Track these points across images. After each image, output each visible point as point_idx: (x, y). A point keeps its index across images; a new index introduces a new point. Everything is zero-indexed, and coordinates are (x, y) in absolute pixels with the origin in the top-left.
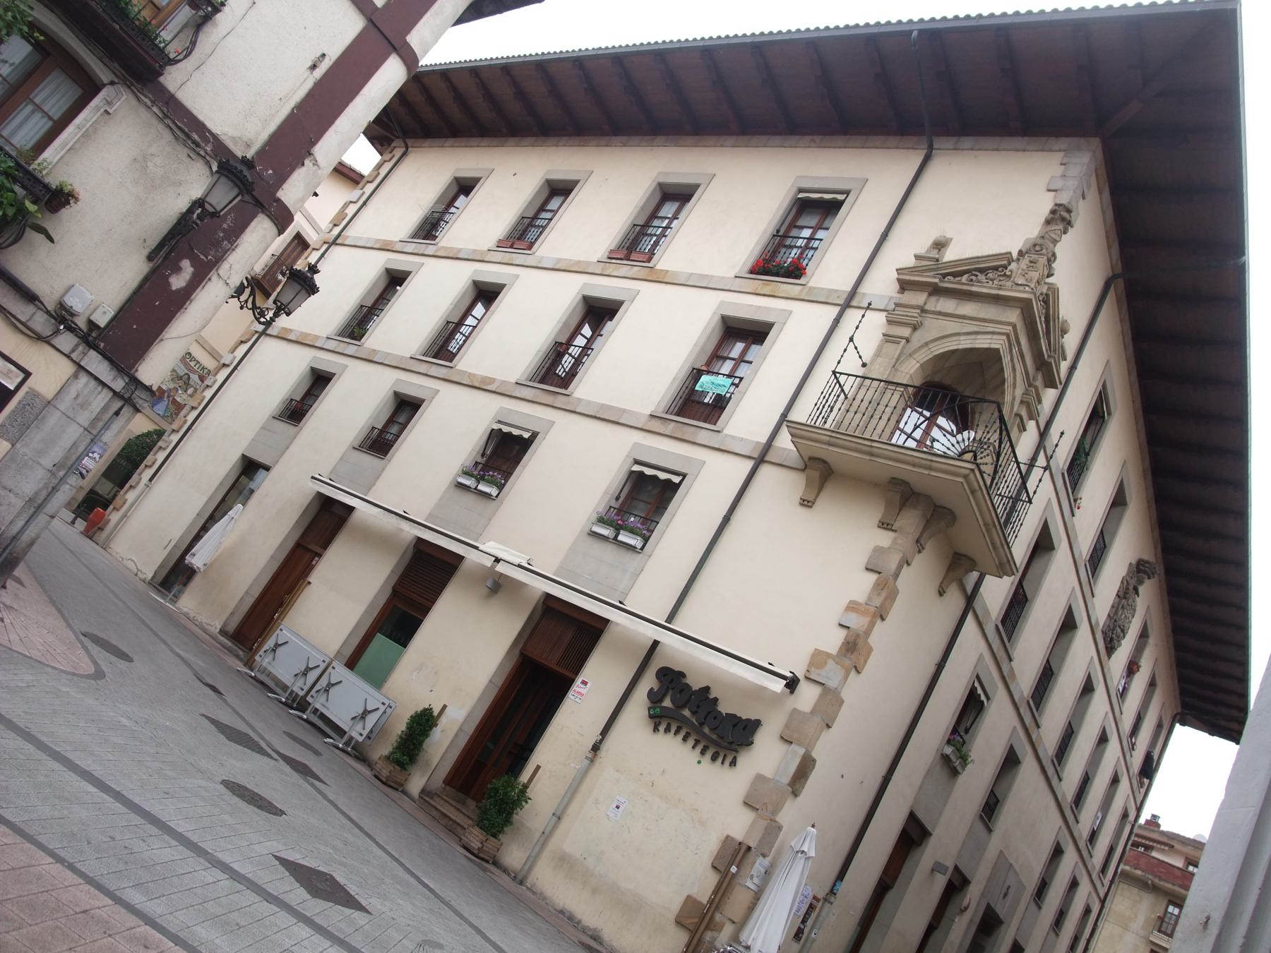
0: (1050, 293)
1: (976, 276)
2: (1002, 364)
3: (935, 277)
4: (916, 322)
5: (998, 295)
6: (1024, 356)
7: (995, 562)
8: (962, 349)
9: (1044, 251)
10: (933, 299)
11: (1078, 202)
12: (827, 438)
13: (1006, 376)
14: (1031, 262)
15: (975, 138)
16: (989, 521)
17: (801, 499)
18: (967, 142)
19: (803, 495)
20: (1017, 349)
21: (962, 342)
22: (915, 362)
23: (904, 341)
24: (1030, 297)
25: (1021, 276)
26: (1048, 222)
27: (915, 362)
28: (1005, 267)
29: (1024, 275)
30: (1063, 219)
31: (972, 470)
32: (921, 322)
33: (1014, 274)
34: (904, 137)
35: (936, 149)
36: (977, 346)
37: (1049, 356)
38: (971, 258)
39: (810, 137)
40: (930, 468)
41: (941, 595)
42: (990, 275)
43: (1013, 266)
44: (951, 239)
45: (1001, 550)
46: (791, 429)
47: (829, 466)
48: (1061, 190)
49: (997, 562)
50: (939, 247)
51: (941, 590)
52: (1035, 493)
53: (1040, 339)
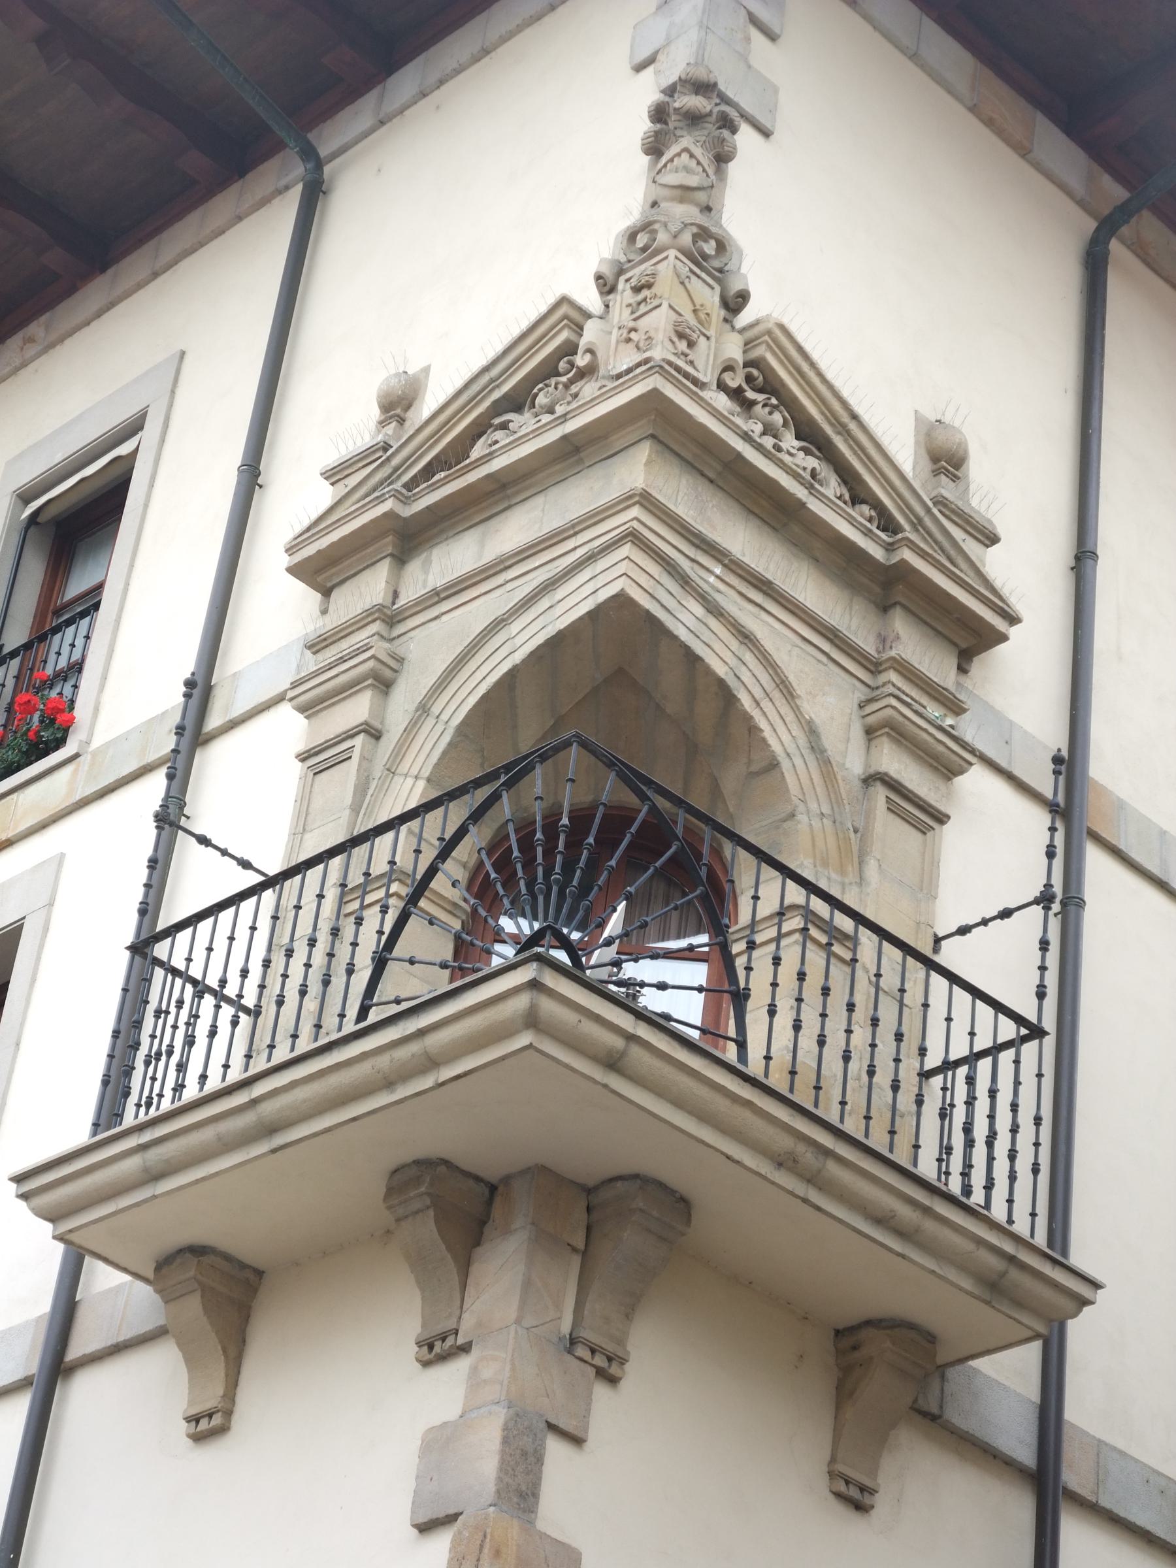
0: (760, 351)
1: (504, 426)
2: (675, 638)
3: (381, 500)
4: (371, 663)
5: (565, 438)
6: (769, 583)
7: (961, 1289)
8: (525, 661)
9: (662, 237)
10: (414, 568)
11: (744, 58)
12: (133, 1164)
13: (720, 670)
14: (637, 290)
15: (419, 60)
16: (785, 1142)
17: (188, 1420)
18: (405, 81)
19: (191, 1403)
20: (718, 570)
21: (519, 641)
22: (410, 781)
23: (359, 741)
24: (650, 388)
25: (622, 346)
26: (655, 148)
27: (410, 781)
28: (570, 349)
29: (629, 340)
30: (694, 119)
31: (534, 985)
32: (393, 656)
33: (600, 355)
34: (250, 176)
35: (334, 156)
36: (562, 624)
37: (890, 548)
38: (467, 386)
39: (20, 336)
40: (432, 1062)
41: (860, 1508)
42: (542, 400)
43: (591, 333)
44: (426, 370)
45: (929, 1225)
46: (40, 1201)
47: (227, 1257)
48: (668, 43)
49: (967, 1284)
50: (398, 411)
51: (842, 1487)
52: (246, 865)
53: (803, 505)
